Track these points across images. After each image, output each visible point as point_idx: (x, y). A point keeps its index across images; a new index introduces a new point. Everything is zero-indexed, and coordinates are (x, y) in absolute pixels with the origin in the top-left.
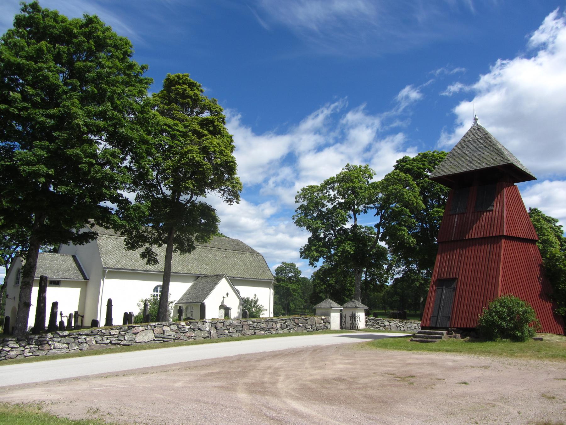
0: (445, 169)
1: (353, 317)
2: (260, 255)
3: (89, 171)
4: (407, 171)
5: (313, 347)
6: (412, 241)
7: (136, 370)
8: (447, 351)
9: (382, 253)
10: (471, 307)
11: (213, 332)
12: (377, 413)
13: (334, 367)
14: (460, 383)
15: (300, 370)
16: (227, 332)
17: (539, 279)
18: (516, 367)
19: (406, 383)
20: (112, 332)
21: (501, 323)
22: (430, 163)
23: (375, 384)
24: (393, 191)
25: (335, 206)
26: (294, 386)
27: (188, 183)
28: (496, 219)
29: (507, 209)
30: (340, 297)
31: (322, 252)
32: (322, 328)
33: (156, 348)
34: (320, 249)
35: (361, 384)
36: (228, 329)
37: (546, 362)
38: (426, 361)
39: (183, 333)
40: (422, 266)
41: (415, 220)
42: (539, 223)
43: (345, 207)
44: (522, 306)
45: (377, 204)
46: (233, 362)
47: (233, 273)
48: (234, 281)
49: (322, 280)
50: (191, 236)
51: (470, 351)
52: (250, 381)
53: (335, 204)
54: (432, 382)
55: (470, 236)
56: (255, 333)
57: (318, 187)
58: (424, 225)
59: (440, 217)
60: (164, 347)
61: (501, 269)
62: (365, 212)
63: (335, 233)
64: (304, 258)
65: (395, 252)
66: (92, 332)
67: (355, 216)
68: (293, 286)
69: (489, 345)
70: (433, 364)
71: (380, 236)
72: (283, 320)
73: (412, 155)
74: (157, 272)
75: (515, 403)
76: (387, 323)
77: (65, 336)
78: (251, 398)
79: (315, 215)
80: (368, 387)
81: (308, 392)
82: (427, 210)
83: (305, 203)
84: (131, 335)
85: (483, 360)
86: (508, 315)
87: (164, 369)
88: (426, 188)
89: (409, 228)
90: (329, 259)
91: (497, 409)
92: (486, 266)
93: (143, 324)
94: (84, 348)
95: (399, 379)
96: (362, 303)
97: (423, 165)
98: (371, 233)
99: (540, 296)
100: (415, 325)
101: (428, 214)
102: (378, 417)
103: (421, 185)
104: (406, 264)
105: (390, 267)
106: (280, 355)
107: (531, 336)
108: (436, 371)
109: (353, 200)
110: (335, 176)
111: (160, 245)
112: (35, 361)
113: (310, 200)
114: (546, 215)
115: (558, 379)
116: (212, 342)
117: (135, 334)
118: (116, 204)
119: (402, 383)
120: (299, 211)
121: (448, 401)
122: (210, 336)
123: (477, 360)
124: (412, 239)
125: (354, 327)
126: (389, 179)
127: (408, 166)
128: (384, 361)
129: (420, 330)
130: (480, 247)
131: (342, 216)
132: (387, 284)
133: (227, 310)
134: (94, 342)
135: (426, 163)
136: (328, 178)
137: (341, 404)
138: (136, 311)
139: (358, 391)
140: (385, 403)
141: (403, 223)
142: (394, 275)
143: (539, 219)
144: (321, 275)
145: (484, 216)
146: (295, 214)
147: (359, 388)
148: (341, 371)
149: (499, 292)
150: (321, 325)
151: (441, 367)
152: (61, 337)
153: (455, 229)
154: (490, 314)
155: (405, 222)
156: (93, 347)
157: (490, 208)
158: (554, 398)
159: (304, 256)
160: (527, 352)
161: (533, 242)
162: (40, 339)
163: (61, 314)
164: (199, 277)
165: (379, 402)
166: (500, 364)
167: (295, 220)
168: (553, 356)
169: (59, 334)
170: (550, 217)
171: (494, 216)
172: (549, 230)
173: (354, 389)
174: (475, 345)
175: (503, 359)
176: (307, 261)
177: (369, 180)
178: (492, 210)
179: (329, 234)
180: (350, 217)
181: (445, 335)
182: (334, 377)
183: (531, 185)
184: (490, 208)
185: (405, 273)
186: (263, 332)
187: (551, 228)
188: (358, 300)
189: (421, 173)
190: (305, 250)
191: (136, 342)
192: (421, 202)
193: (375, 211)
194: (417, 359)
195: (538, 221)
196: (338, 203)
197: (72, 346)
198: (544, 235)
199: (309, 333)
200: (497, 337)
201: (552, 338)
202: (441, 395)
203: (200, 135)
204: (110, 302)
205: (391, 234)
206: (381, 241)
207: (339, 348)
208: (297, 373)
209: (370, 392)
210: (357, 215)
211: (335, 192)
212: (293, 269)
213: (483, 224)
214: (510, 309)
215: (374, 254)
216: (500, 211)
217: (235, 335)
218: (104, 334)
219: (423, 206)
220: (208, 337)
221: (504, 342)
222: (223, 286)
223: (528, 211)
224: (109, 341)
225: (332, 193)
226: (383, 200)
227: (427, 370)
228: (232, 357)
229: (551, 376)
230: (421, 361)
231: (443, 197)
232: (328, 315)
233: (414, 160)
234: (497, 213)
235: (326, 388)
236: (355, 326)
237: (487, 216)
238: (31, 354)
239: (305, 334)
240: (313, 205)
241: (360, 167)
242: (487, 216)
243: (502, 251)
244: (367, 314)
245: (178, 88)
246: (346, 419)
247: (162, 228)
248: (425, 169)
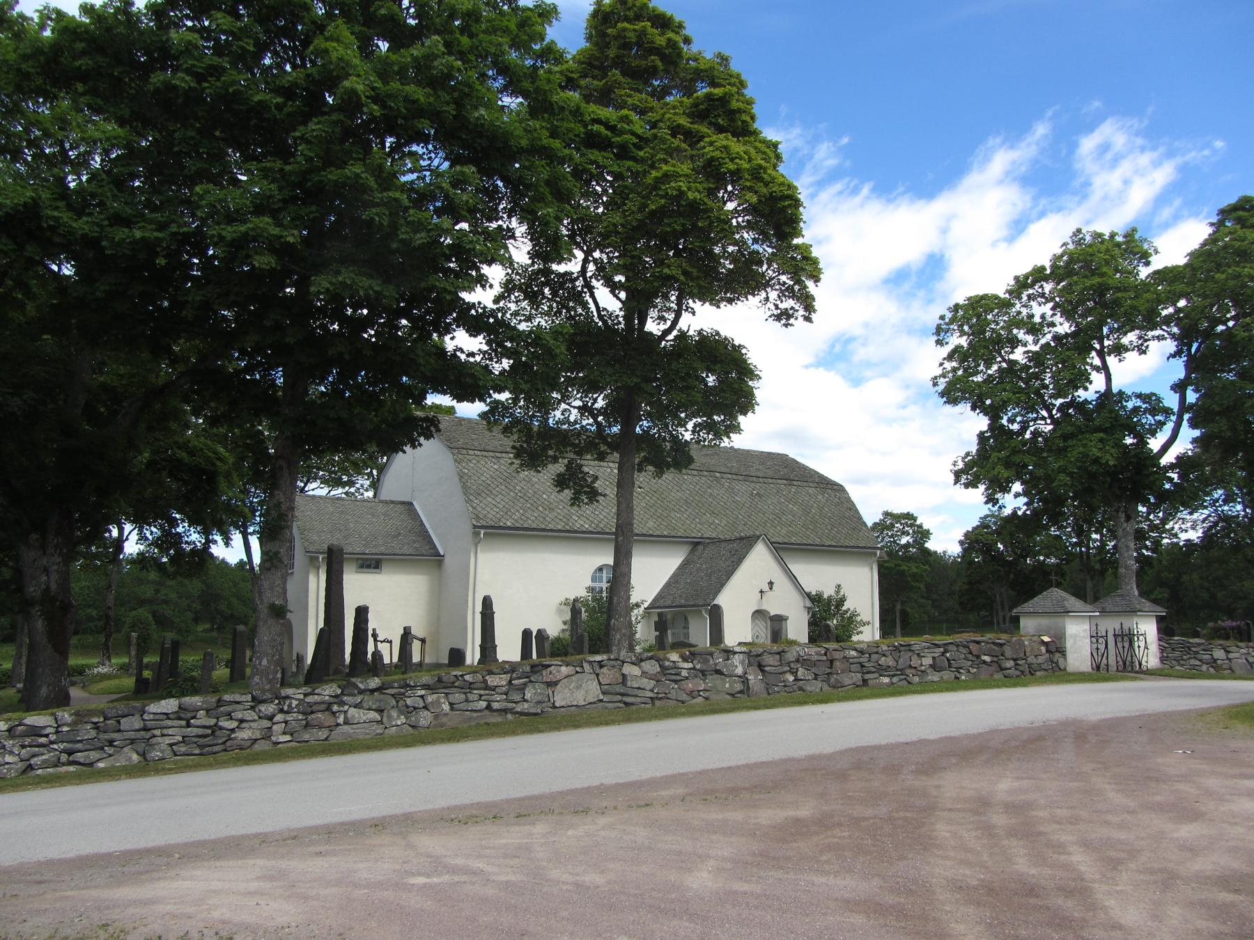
3: (394, 227)
7: (553, 797)
11: (754, 678)
16: (791, 678)
20: (492, 680)
24: (1231, 283)
27: (669, 266)
30: (1091, 581)
33: (607, 723)
36: (795, 673)
39: (676, 682)
46: (842, 776)
47: (781, 534)
48: (781, 550)
50: (681, 430)
56: (865, 682)
60: (628, 719)
63: (1051, 416)
66: (440, 680)
72: (938, 646)
74: (599, 533)
76: (1219, 654)
77: (372, 691)
84: (540, 688)
87: (634, 796)
93: (568, 659)
94: (423, 722)
111: (601, 457)
112: (294, 758)
113: (978, 331)
116: (756, 708)
117: (552, 684)
118: (480, 338)
122: (746, 690)
133: (777, 623)
134: (446, 707)
138: (554, 626)
152: (361, 692)
156: (444, 720)
162: (309, 699)
163: (375, 635)
164: (697, 544)
167: (941, 387)
169: (356, 687)
186: (886, 680)
191: (555, 707)
197: (390, 717)
203: (693, 138)
204: (487, 603)
217: (815, 687)
218: (471, 686)
220: (741, 692)
222: (759, 562)
224: (483, 704)
228: (831, 757)
238: (288, 738)
241: (1112, 235)
244: (1165, 630)
245: (624, 30)
247: (601, 412)
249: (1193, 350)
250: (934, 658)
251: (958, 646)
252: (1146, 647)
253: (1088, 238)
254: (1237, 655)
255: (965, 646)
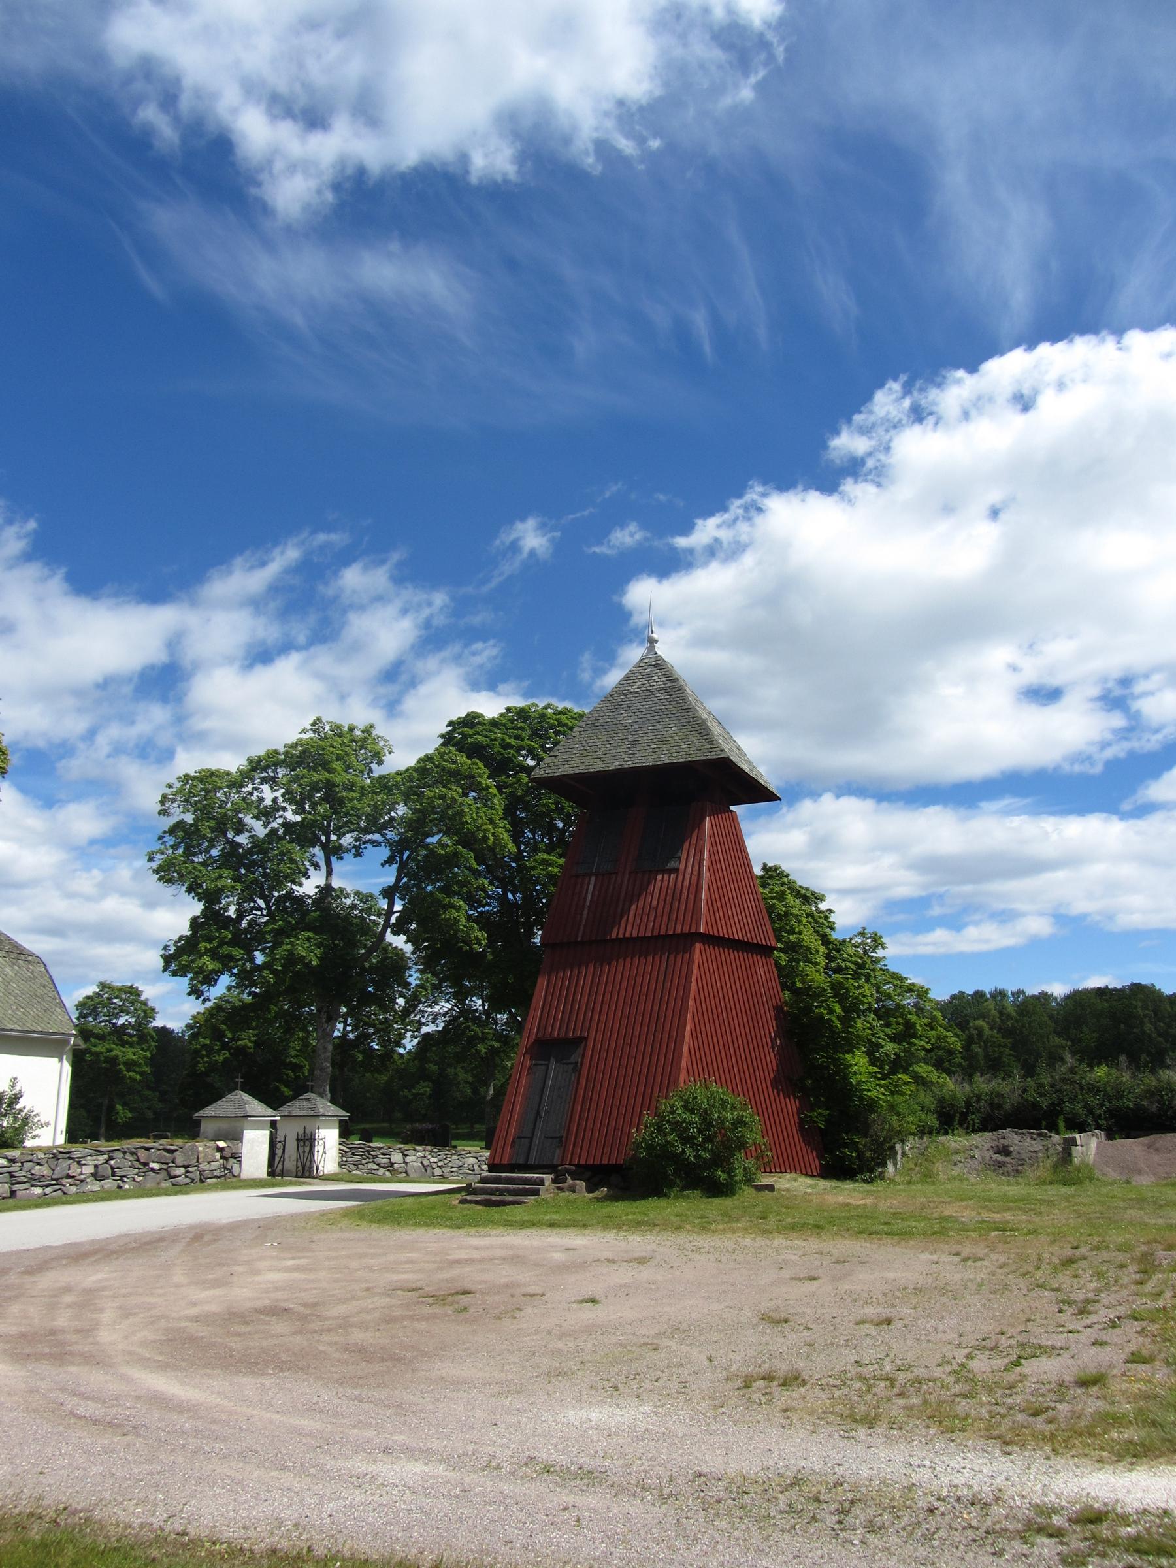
0: (571, 758)
1: (307, 1142)
2: (36, 960)
4: (475, 751)
5: (192, 1227)
6: (477, 938)
8: (552, 1225)
9: (395, 966)
10: (615, 1110)
12: (379, 1385)
13: (258, 1278)
14: (581, 1302)
15: (161, 1291)
17: (773, 1041)
18: (711, 1256)
19: (449, 1310)
21: (683, 1152)
22: (534, 734)
23: (369, 1317)
24: (437, 802)
25: (274, 832)
26: (147, 1334)
28: (685, 891)
29: (713, 870)
30: (274, 1083)
31: (230, 957)
32: (217, 1173)
34: (225, 950)
35: (336, 1318)
37: (778, 1241)
38: (499, 1253)
40: (496, 1003)
41: (486, 882)
42: (784, 903)
43: (303, 834)
44: (733, 1108)
45: (390, 834)
49: (218, 1035)
51: (608, 1223)
52: (14, 1330)
53: (275, 825)
54: (516, 1302)
55: (622, 931)
56: (13, 1194)
57: (228, 774)
58: (510, 896)
59: (550, 876)
61: (689, 1016)
62: (358, 854)
63: (268, 907)
64: (175, 973)
65: (428, 964)
67: (328, 863)
68: (130, 1054)
69: (653, 1207)
70: (516, 1259)
71: (393, 920)
72: (102, 1153)
73: (490, 707)
75: (703, 1338)
76: (397, 1158)
78: (23, 1373)
79: (215, 852)
80: (351, 1326)
81: (185, 1348)
82: (518, 857)
83: (189, 818)
85: (637, 1242)
86: (700, 1132)
88: (520, 799)
89: (471, 901)
90: (246, 978)
91: (663, 1355)
92: (656, 1008)
95: (431, 1300)
96: (333, 1101)
97: (518, 738)
98: (369, 910)
99: (775, 1083)
100: (471, 1159)
101: (521, 868)
102: (382, 1394)
103: (508, 790)
104: (455, 996)
105: (413, 1003)
106: (95, 1252)
107: (749, 1180)
108: (526, 1278)
109: (325, 817)
110: (282, 750)
113: (204, 811)
114: (799, 883)
115: (800, 1279)
119: (438, 1310)
120: (170, 840)
121: (550, 1346)
123: (623, 1244)
124: (478, 933)
125: (306, 1170)
126: (425, 769)
127: (479, 738)
128: (391, 1258)
129: (485, 1174)
130: (643, 960)
131: (292, 861)
132: (401, 1050)
135: (525, 735)
136: (259, 751)
137: (282, 1370)
139: (326, 1337)
140: (397, 1360)
141: (456, 888)
142: (420, 1024)
143: (783, 892)
144: (210, 1025)
145: (658, 884)
146: (158, 846)
147: (329, 1330)
148: (277, 1289)
149: (683, 1074)
150: (214, 1165)
151: (537, 1265)
153: (586, 912)
154: (660, 1129)
155: (462, 885)
157: (672, 864)
158: (786, 1321)
159: (173, 967)
160: (738, 1221)
161: (765, 951)
165: (382, 1360)
166: (676, 1252)
167: (155, 865)
168: (793, 1228)
170: (807, 889)
171: (679, 884)
172: (804, 920)
173: (316, 1332)
174: (620, 1208)
175: (685, 1239)
176: (184, 983)
177: (374, 766)
178: (676, 870)
179: (252, 909)
180: (316, 866)
181: (547, 1183)
182: (259, 1304)
183: (769, 813)
184: (672, 864)
185: (452, 1023)
187: (808, 915)
188: (321, 1095)
189: (509, 759)
190: (180, 951)
192: (506, 836)
193: (385, 852)
194: (477, 1248)
195: (781, 897)
196: (283, 825)
198: (792, 931)
199: (178, 1189)
200: (671, 1185)
201: (796, 1184)
202: (536, 1332)
205: (423, 918)
206: (395, 933)
207: (265, 1228)
208: (153, 1300)
209: (358, 1336)
210: (333, 859)
211: (278, 794)
212: (132, 1003)
213: (654, 902)
214: (705, 1114)
215: (373, 969)
216: (695, 873)
219: (512, 847)
221: (688, 1197)
223: (758, 871)
225: (268, 794)
226: (410, 824)
227: (503, 1274)
229: (786, 1274)
230: (485, 1254)
231: (560, 825)
232: (237, 1137)
233: (494, 723)
234: (688, 877)
235: (239, 1335)
236: (311, 1167)
237: (665, 884)
239: (166, 1193)
240: (212, 823)
241: (351, 729)
242: (665, 884)
243: (695, 972)
244: (345, 1132)
246: (299, 1406)
248: (522, 748)
249: (405, 857)
250: (96, 1166)
251: (124, 1153)
252: (324, 1153)
253: (327, 728)
254: (414, 1158)
255: (133, 1154)
